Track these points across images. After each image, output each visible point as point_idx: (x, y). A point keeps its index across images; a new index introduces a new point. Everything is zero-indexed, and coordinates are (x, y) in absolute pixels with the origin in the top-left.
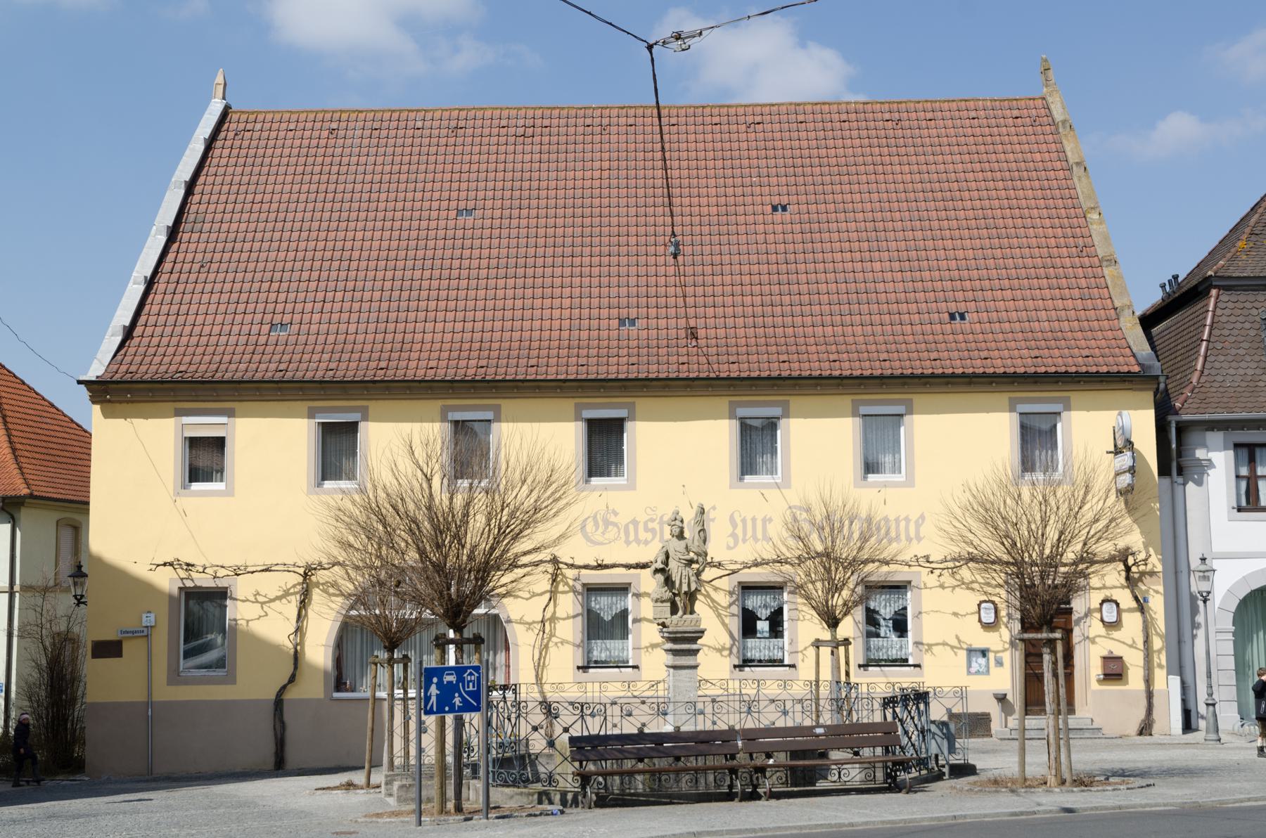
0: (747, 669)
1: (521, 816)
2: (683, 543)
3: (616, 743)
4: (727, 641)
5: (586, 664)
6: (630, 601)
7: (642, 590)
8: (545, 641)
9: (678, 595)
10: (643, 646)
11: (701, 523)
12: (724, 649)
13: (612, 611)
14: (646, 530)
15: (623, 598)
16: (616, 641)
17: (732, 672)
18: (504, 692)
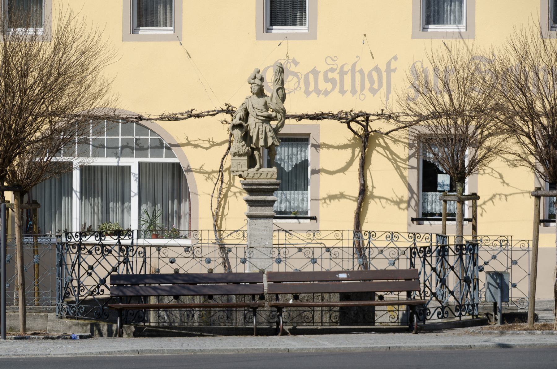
0: (426, 222)
1: (38, 339)
2: (262, 101)
3: (154, 282)
4: (406, 195)
5: (548, 219)
6: (310, 152)
7: (321, 141)
8: (224, 191)
9: (257, 149)
10: (320, 198)
11: (280, 81)
12: (401, 201)
13: (292, 161)
14: (326, 80)
15: (303, 149)
16: (300, 192)
17: (409, 225)
18: (119, 237)
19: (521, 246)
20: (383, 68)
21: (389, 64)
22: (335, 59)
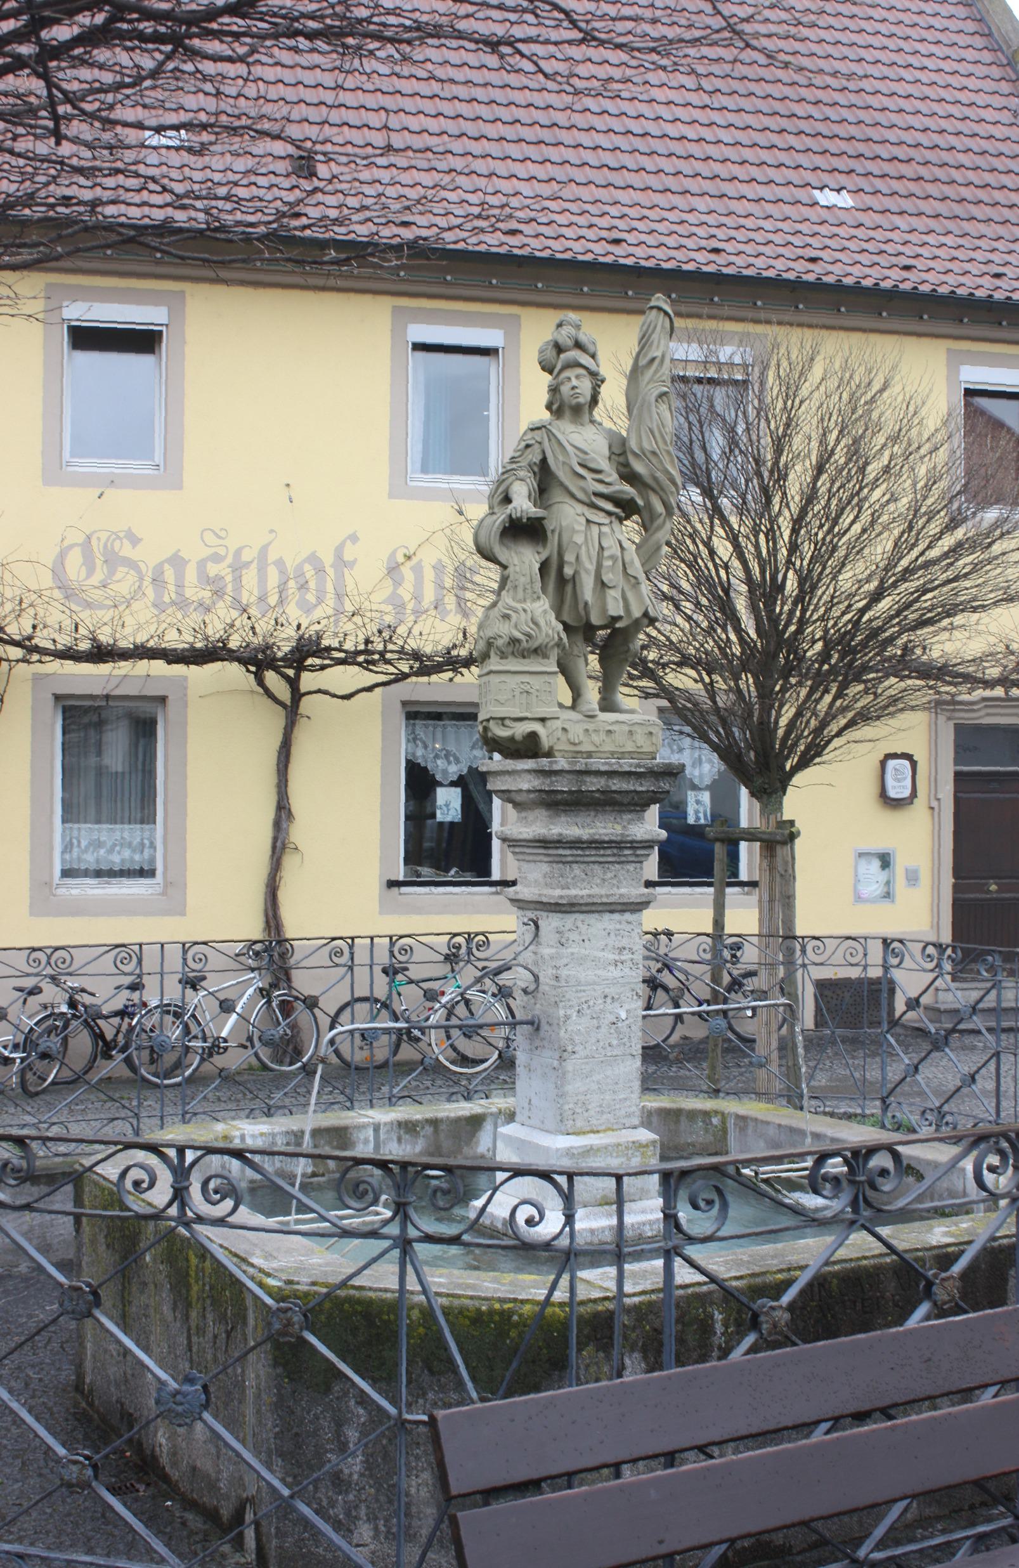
19: (848, 957)
20: (328, 559)
21: (339, 551)
22: (223, 534)
